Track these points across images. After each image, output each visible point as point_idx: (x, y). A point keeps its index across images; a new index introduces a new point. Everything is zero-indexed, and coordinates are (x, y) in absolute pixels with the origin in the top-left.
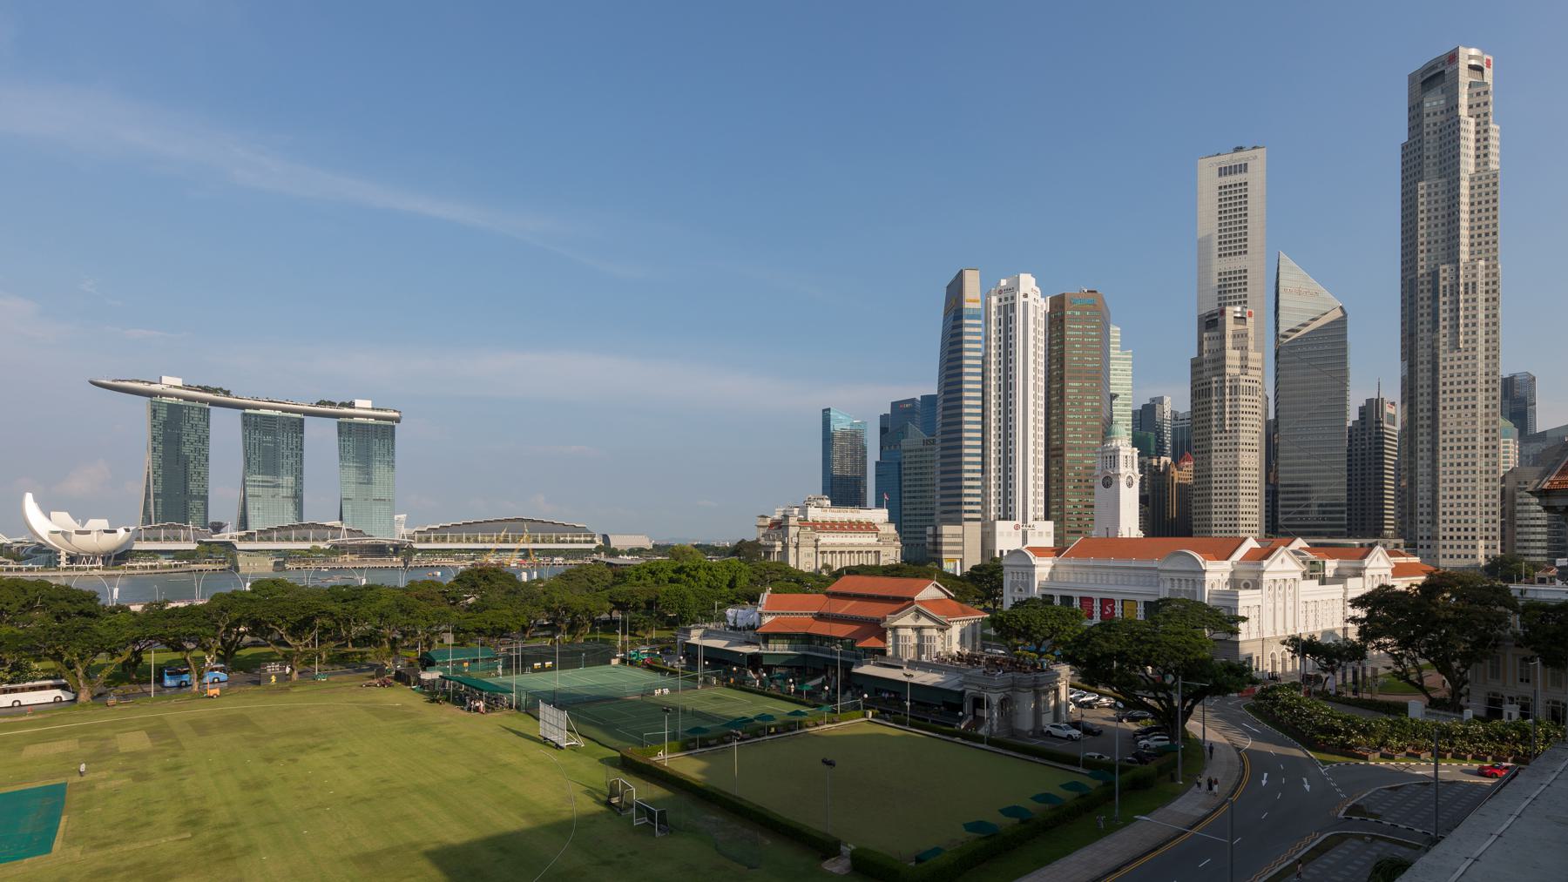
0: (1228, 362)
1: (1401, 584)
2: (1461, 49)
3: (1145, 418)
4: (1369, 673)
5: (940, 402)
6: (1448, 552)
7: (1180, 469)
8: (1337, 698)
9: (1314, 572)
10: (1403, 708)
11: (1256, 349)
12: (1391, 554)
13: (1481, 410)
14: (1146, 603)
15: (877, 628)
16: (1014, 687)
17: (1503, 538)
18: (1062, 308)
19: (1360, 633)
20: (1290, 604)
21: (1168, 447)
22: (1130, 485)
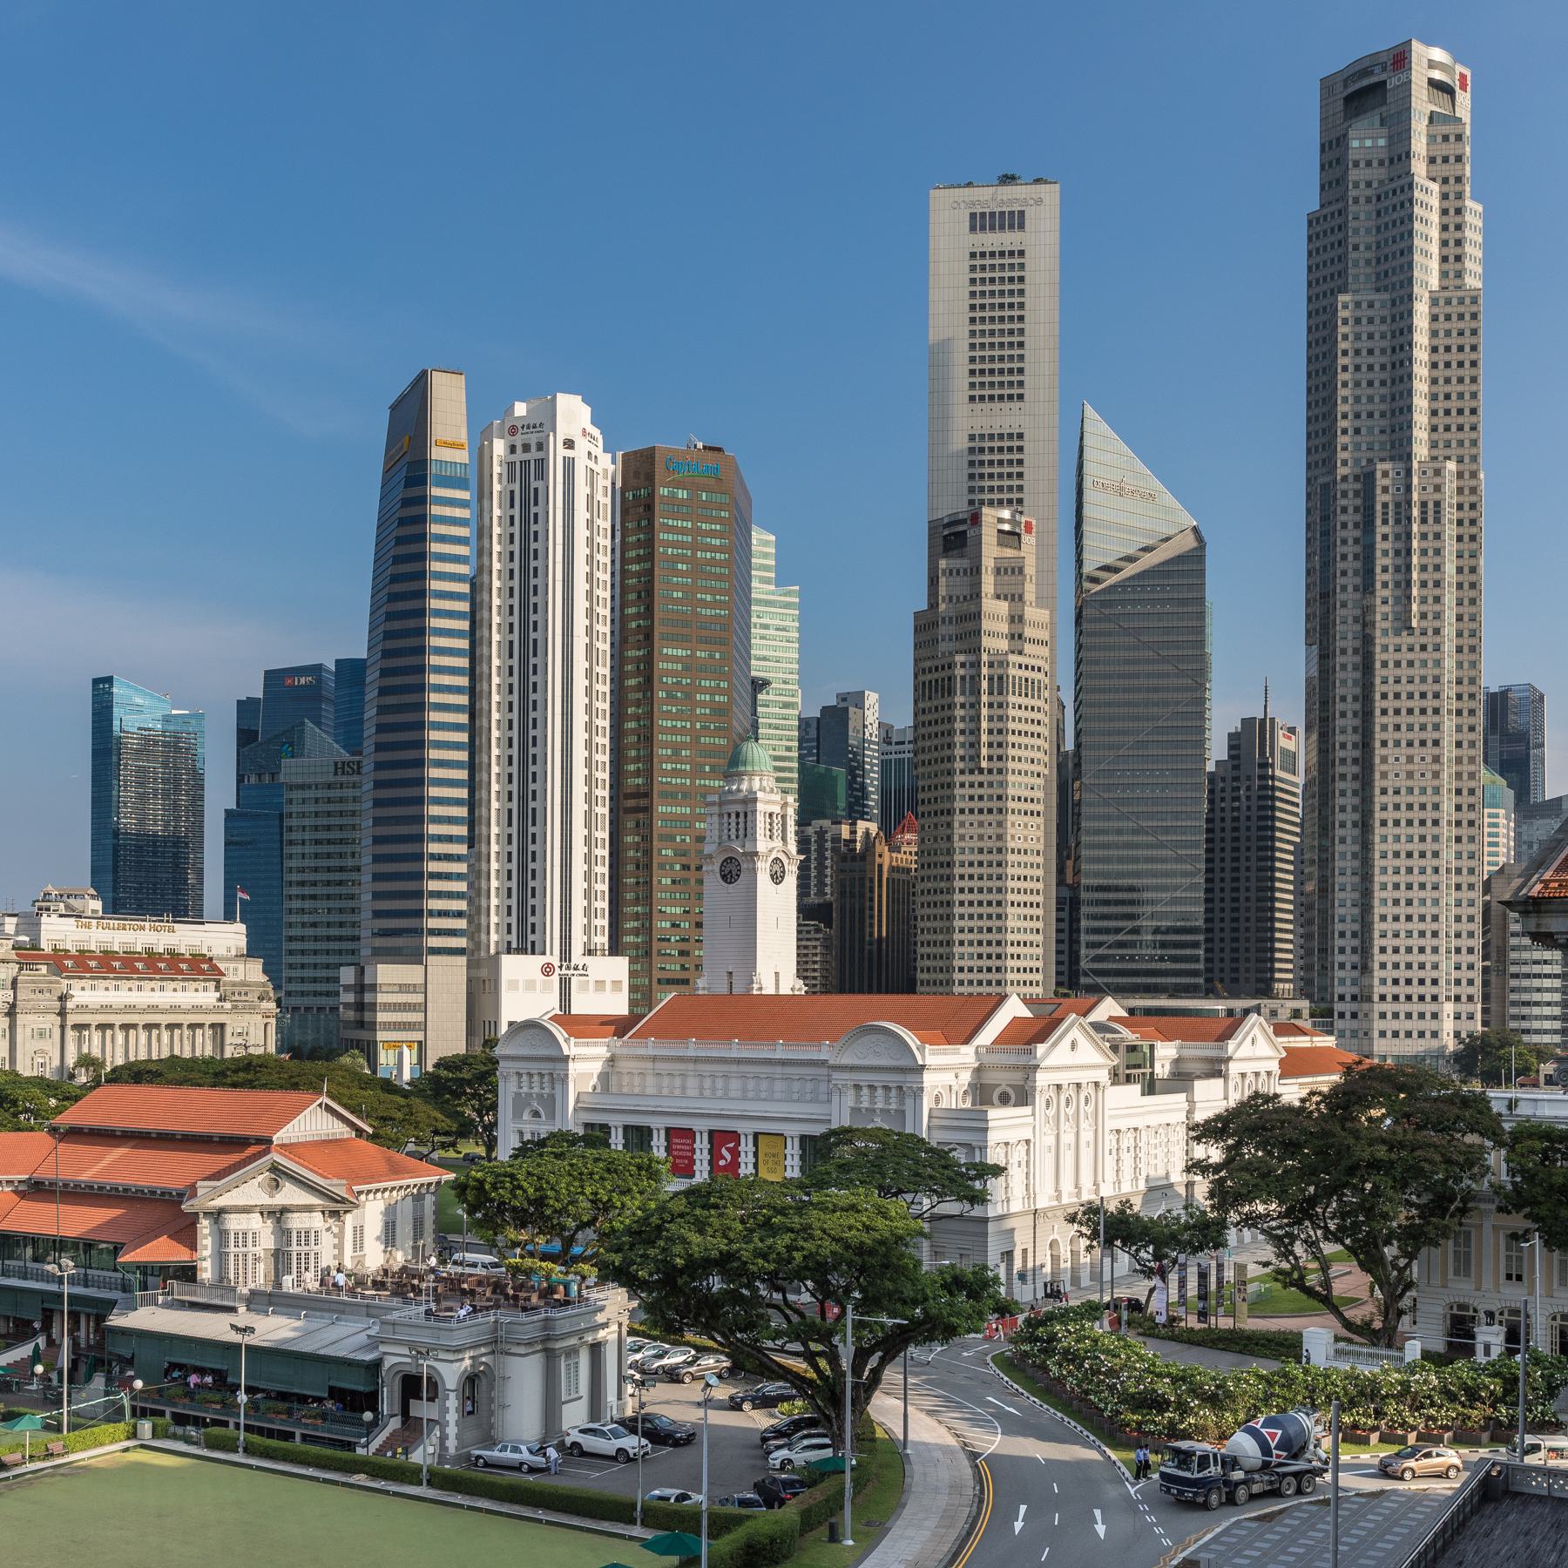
0: (986, 625)
1: (1291, 1092)
2: (1416, 45)
3: (826, 735)
4: (1229, 1274)
5: (372, 676)
6: (1390, 1025)
7: (895, 849)
8: (1171, 1332)
9: (1132, 1068)
10: (1289, 1346)
11: (1040, 602)
12: (1280, 1030)
13: (1448, 751)
14: (803, 1139)
15: (172, 1213)
16: (497, 1343)
17: (1486, 998)
18: (650, 478)
19: (1212, 1195)
20: (1087, 1136)
21: (874, 799)
22: (777, 878)
